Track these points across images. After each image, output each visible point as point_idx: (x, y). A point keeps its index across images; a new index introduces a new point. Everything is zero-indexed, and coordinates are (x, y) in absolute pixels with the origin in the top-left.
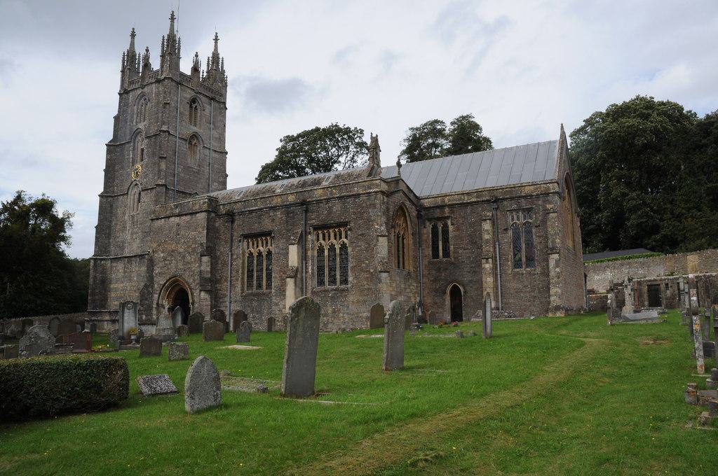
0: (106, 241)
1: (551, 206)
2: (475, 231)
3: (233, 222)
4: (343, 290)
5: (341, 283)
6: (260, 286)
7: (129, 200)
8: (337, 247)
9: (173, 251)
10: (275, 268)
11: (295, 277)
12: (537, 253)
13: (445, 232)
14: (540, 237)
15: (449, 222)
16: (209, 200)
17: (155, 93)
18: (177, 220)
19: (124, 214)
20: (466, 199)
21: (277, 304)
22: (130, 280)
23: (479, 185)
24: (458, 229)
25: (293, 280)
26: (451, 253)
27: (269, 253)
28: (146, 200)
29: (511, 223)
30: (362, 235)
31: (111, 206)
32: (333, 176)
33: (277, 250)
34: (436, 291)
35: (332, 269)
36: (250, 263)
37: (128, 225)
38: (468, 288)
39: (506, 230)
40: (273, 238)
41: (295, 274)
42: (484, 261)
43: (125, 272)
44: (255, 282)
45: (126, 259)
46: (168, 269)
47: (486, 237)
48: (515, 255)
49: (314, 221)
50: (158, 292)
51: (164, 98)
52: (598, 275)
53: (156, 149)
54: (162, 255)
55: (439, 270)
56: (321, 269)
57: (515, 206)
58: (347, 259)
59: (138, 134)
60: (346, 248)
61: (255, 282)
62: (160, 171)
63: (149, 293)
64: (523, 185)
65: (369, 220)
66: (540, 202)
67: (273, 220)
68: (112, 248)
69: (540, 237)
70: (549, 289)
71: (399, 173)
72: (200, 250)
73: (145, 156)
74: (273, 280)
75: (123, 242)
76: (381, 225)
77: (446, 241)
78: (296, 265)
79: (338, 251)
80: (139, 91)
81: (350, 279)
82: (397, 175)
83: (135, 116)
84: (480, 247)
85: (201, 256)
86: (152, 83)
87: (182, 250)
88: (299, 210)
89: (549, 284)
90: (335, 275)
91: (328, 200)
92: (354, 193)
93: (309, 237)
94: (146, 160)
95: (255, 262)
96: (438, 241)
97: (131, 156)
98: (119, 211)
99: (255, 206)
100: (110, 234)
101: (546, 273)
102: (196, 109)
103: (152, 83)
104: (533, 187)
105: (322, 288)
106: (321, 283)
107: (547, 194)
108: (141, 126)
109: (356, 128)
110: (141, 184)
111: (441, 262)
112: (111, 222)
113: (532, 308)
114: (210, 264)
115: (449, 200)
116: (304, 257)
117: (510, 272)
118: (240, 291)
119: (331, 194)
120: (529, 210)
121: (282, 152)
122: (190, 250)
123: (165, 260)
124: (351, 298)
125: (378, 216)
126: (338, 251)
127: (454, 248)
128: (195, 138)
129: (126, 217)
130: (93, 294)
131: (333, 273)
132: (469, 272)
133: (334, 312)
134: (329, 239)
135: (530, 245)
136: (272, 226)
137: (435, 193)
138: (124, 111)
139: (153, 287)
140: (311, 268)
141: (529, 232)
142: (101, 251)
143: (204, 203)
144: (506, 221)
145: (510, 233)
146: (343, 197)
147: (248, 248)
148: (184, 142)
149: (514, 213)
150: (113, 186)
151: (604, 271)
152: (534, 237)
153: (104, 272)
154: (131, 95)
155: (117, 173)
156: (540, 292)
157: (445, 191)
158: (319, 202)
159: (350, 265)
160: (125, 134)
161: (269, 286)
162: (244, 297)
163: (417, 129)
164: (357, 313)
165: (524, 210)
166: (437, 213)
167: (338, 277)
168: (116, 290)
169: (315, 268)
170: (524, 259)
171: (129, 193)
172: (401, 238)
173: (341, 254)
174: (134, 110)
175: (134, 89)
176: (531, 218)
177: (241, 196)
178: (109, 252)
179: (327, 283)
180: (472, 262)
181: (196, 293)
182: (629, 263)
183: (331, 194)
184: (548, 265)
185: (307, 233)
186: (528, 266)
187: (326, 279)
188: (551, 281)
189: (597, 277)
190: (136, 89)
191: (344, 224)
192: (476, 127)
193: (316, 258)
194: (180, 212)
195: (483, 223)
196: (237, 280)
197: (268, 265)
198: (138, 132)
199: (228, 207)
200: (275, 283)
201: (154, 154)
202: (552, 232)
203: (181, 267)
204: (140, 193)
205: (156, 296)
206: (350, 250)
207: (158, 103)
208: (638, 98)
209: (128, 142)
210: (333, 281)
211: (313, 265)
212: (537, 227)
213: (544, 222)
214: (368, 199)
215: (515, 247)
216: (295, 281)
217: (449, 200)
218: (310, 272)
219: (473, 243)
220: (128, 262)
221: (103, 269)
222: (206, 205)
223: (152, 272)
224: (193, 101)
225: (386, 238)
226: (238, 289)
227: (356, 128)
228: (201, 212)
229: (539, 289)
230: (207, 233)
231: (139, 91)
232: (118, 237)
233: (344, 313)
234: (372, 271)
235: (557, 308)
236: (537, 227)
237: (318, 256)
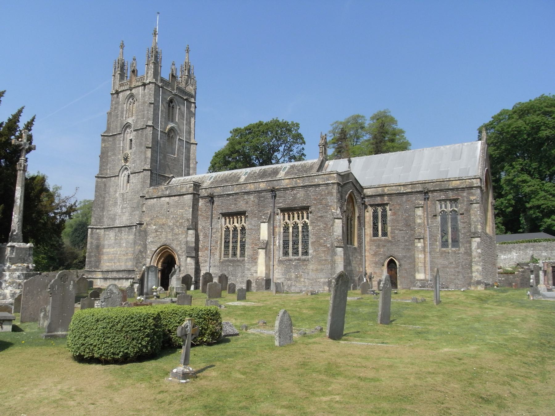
0: (101, 214)
1: (474, 198)
2: (409, 216)
3: (213, 203)
4: (305, 260)
5: (303, 254)
6: (235, 254)
7: (120, 181)
8: (300, 226)
9: (163, 225)
10: (248, 240)
11: (265, 248)
12: (461, 236)
13: (384, 216)
14: (464, 223)
15: (388, 208)
16: (194, 184)
17: (142, 94)
18: (167, 199)
19: (116, 192)
20: (402, 190)
21: (249, 270)
22: (120, 246)
23: (411, 179)
24: (394, 214)
25: (264, 250)
26: (389, 234)
27: (243, 229)
28: (135, 182)
29: (440, 210)
30: (321, 217)
31: (105, 185)
32: (289, 167)
33: (250, 227)
34: (376, 263)
35: (295, 243)
36: (227, 236)
37: (119, 202)
38: (402, 262)
39: (435, 216)
40: (247, 216)
41: (266, 246)
42: (416, 241)
43: (116, 239)
44: (230, 251)
45: (117, 229)
46: (159, 238)
47: (419, 221)
48: (442, 237)
49: (281, 204)
50: (150, 257)
51: (149, 99)
52: (504, 254)
53: (142, 140)
54: (154, 227)
55: (378, 246)
56: (286, 243)
57: (443, 197)
58: (308, 235)
59: (127, 127)
60: (307, 226)
61: (230, 251)
62: (146, 158)
63: (143, 257)
64: (451, 179)
65: (327, 205)
66: (465, 194)
67: (247, 203)
68: (105, 220)
69: (464, 223)
70: (471, 266)
71: (349, 168)
72: (186, 224)
73: (133, 145)
74: (246, 250)
75: (115, 215)
76: (337, 210)
77: (384, 223)
78: (267, 239)
79: (300, 229)
80: (128, 92)
81: (311, 251)
82: (348, 169)
83: (125, 113)
84: (413, 229)
85: (188, 229)
86: (139, 86)
87: (171, 224)
88: (269, 195)
89: (471, 262)
90: (298, 248)
91: (293, 188)
92: (315, 183)
93: (277, 216)
94: (134, 149)
95: (231, 235)
96: (377, 223)
97: (122, 145)
98: (112, 190)
99: (232, 191)
100: (103, 208)
101: (469, 253)
102: (173, 108)
103: (139, 86)
104: (459, 181)
105: (287, 258)
106: (286, 253)
107: (471, 188)
108: (130, 121)
109: (292, 122)
110: (130, 168)
111: (380, 240)
112: (104, 198)
113: (457, 281)
114: (194, 235)
115: (388, 190)
116: (272, 233)
117: (438, 250)
118: (218, 258)
119: (296, 183)
120: (456, 200)
121: (232, 143)
122: (178, 224)
123: (157, 231)
124: (311, 267)
125: (334, 202)
126: (300, 229)
127: (392, 229)
128: (172, 131)
129: (117, 195)
130: (90, 257)
131: (296, 246)
132: (403, 249)
133: (297, 277)
134: (293, 219)
135: (455, 229)
136: (246, 207)
137: (376, 184)
138: (115, 108)
139: (146, 253)
140: (279, 241)
141: (454, 220)
142: (97, 221)
143: (190, 187)
144: (435, 209)
145: (439, 218)
146: (306, 186)
147: (225, 224)
148: (164, 135)
149: (443, 202)
150: (107, 169)
151: (510, 251)
152: (459, 222)
153: (98, 239)
154: (121, 95)
155: (109, 159)
156: (463, 268)
157: (383, 183)
158: (286, 189)
159: (310, 241)
160: (116, 127)
161: (243, 255)
162: (222, 263)
163: (341, 123)
164: (316, 279)
165: (451, 200)
166: (378, 200)
167: (300, 249)
168: (108, 253)
169: (281, 242)
170: (450, 241)
171: (120, 175)
172: (349, 220)
173: (303, 232)
174: (124, 107)
175: (124, 91)
176: (456, 207)
177: (212, 180)
178: (103, 222)
179: (291, 254)
180: (406, 241)
181: (183, 258)
182: (533, 246)
183: (296, 183)
184: (470, 246)
185: (274, 214)
186: (453, 246)
187: (290, 251)
188: (473, 260)
189: (503, 257)
190: (126, 90)
191: (306, 208)
192: (393, 121)
193: (282, 234)
194: (169, 194)
195: (416, 209)
196: (216, 249)
197: (242, 238)
198: (128, 126)
199: (209, 191)
200: (248, 252)
201: (141, 144)
202: (475, 220)
203: (171, 237)
204: (129, 176)
205: (149, 260)
206: (310, 228)
207: (144, 102)
208: (542, 96)
209: (119, 134)
210: (296, 253)
211: (280, 239)
212: (461, 214)
213: (468, 211)
214: (326, 189)
215: (443, 231)
216: (266, 251)
217: (388, 190)
218: (278, 244)
219: (407, 225)
220: (119, 231)
221: (98, 237)
222: (192, 189)
223: (146, 240)
224: (171, 101)
225: (341, 220)
226: (217, 256)
227: (292, 122)
228: (188, 194)
229: (462, 266)
230: (193, 211)
231: (128, 92)
232: (110, 211)
233: (305, 278)
234: (328, 245)
235: (478, 283)
236: (461, 214)
237: (284, 232)
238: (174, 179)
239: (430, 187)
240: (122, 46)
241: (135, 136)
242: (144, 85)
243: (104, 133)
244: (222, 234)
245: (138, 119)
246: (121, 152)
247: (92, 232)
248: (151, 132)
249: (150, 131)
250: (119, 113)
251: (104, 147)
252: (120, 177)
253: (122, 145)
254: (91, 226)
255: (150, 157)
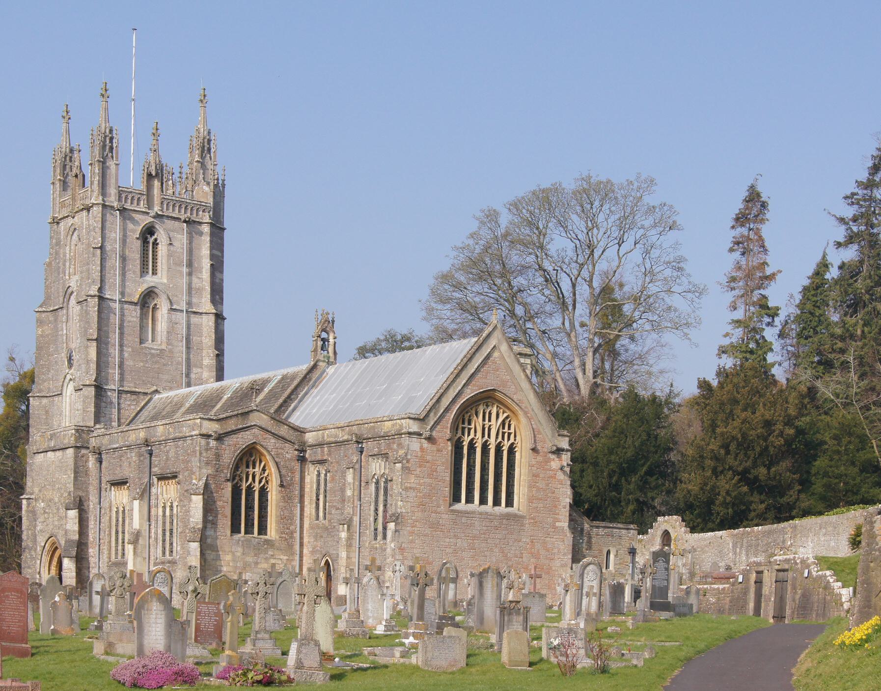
7: (64, 405)
16: (77, 431)
31: (47, 412)
83: (67, 264)
97: (65, 332)
102: (155, 244)
154: (62, 224)
171: (64, 394)
238: (157, 396)
239: (365, 431)
240: (67, 116)
241: (79, 315)
242: (88, 209)
243: (41, 306)
244: (110, 517)
245: (82, 278)
246: (65, 345)
247: (29, 505)
248: (96, 309)
249: (94, 307)
250: (61, 265)
251: (42, 336)
252: (64, 398)
253: (65, 332)
254: (27, 494)
255: (95, 359)
